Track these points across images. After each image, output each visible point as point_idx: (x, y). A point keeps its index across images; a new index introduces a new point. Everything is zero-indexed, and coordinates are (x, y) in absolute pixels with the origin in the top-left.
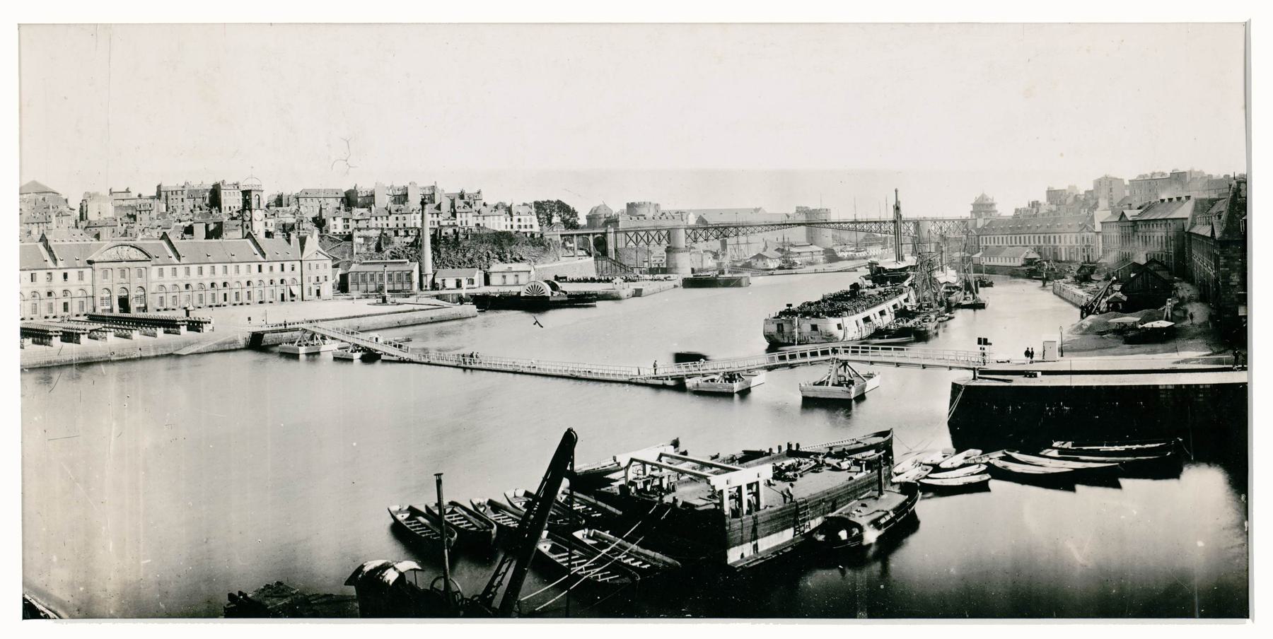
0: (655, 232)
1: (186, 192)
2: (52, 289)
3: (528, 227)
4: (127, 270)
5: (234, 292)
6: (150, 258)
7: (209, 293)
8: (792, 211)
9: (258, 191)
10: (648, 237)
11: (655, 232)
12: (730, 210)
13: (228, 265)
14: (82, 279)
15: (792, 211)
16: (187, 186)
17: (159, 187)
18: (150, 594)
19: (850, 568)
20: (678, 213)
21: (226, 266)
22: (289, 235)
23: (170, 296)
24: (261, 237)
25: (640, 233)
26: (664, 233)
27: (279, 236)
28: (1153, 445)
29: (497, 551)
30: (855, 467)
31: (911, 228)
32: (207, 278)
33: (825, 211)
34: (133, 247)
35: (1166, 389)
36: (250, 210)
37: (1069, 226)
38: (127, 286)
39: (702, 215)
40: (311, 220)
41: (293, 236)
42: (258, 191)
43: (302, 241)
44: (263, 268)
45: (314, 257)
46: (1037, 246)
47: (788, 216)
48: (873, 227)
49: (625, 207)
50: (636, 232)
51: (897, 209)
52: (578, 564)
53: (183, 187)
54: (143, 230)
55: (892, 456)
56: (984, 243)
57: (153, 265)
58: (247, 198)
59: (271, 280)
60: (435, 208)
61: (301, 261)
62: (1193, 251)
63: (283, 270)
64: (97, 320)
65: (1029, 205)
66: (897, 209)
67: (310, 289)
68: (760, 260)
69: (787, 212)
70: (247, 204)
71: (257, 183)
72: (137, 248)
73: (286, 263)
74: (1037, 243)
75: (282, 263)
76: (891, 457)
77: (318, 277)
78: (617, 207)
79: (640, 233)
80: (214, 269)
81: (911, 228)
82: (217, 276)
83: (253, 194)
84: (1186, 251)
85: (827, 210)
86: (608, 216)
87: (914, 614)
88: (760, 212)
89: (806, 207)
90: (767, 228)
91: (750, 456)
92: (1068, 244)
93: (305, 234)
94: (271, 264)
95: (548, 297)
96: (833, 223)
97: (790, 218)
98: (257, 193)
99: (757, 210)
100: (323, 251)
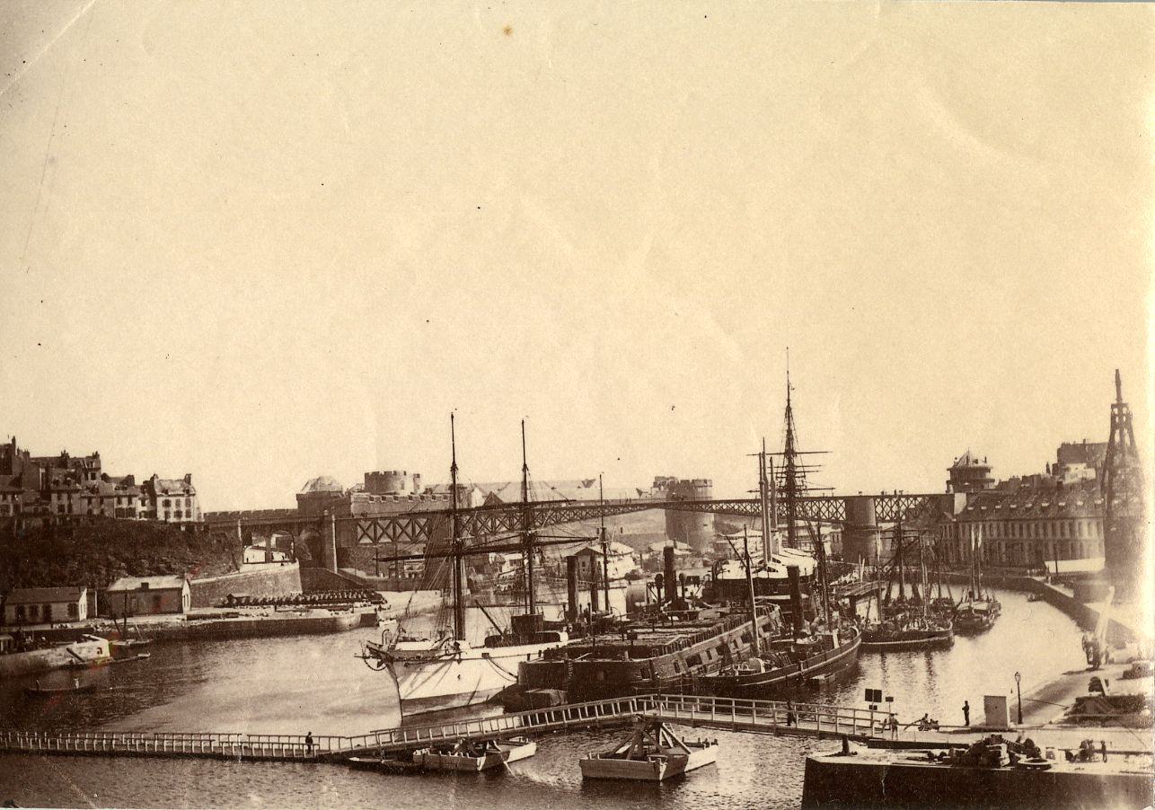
0: (388, 522)
3: (184, 514)
8: (647, 485)
10: (394, 529)
15: (647, 485)
18: (136, 773)
25: (401, 521)
31: (841, 510)
47: (640, 492)
48: (824, 509)
49: (362, 480)
50: (394, 521)
51: (454, 468)
52: (406, 768)
60: (10, 484)
64: (908, 650)
65: (1048, 470)
66: (454, 468)
74: (1059, 536)
79: (401, 521)
81: (841, 510)
84: (271, 522)
85: (705, 481)
91: (944, 732)
97: (643, 496)
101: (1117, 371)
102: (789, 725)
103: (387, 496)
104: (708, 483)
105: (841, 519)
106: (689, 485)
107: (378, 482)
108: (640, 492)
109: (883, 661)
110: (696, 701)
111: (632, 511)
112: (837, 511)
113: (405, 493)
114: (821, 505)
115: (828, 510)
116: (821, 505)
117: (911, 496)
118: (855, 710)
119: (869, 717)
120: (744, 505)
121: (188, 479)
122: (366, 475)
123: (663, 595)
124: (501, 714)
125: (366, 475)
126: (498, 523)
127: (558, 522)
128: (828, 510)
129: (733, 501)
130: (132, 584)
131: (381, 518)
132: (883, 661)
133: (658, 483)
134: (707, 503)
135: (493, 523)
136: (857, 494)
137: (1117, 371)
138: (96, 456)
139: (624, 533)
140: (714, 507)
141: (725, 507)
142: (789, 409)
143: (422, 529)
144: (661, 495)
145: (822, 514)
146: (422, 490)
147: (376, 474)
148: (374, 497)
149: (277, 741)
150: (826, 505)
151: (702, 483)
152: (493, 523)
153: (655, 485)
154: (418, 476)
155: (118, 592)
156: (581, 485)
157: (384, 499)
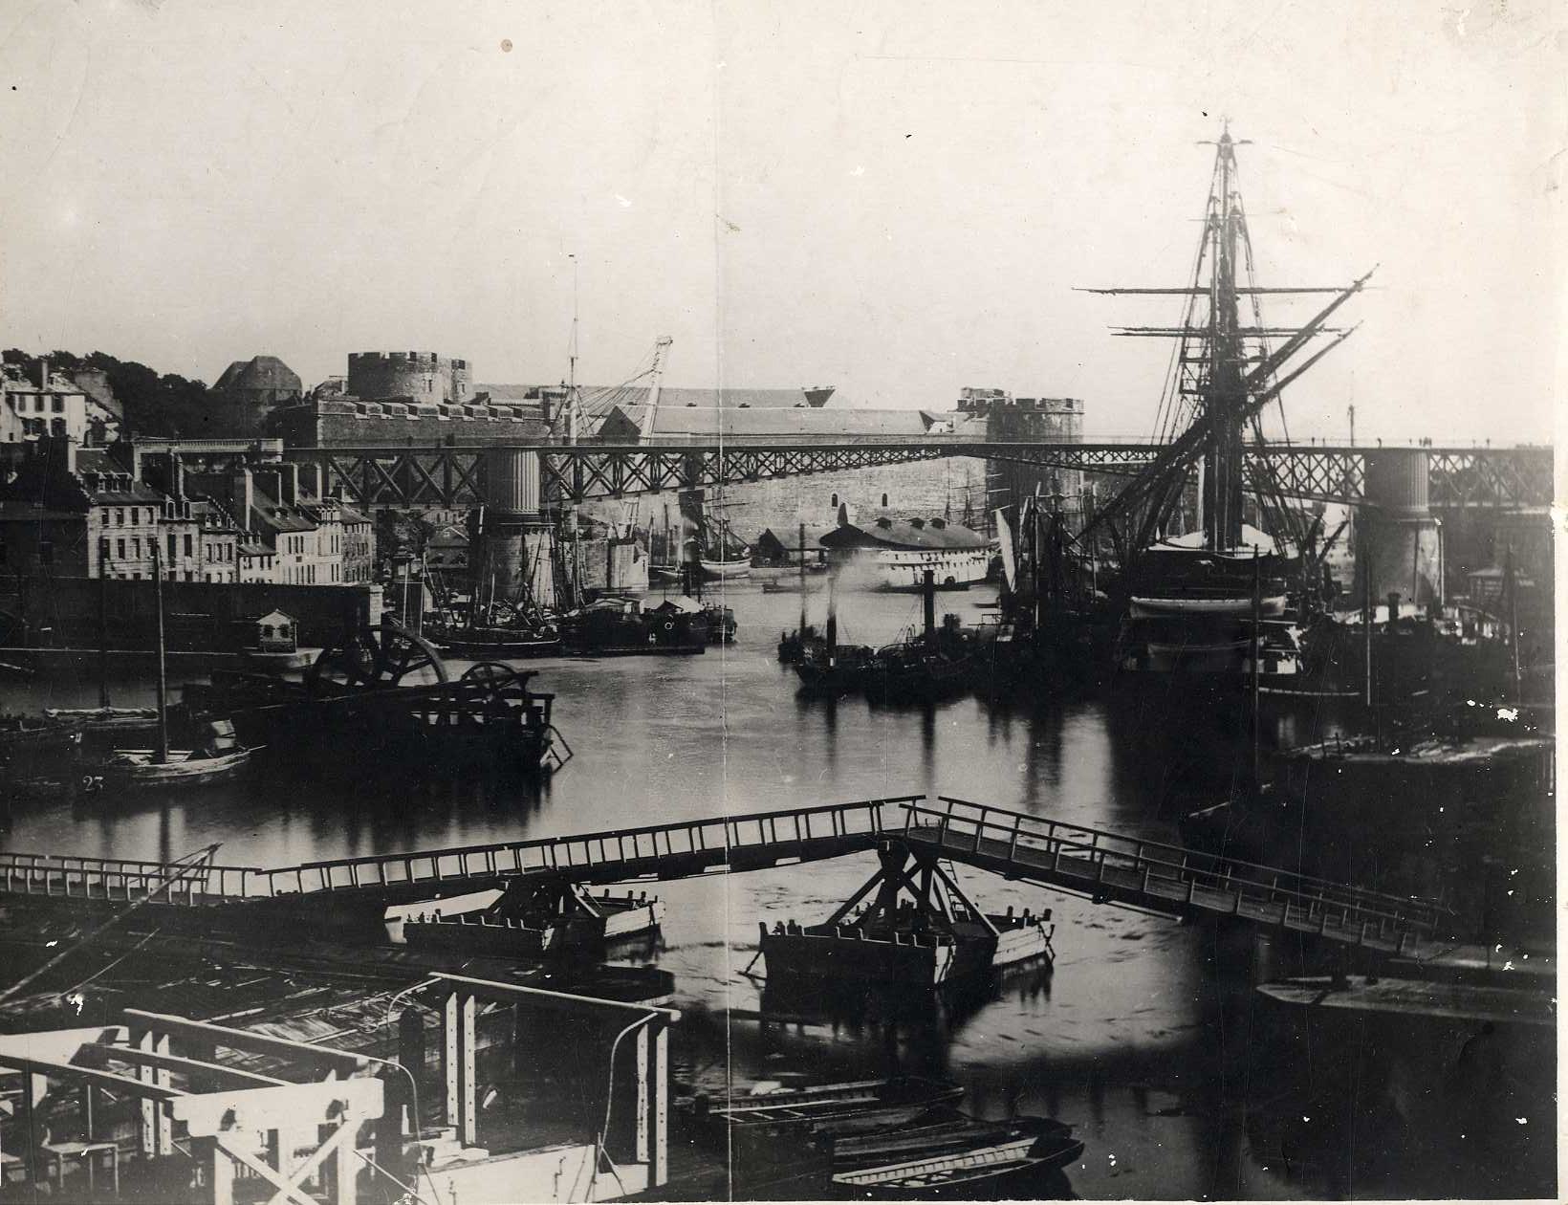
0: (432, 460)
11: (565, 458)
19: (845, 1027)
25: (420, 460)
29: (1015, 988)
30: (1006, 934)
39: (622, 406)
47: (928, 421)
48: (1318, 474)
49: (342, 371)
55: (440, 899)
62: (18, 519)
69: (924, 409)
76: (438, 896)
85: (1069, 403)
86: (283, 396)
87: (62, 1021)
89: (999, 393)
90: (780, 463)
96: (1094, 448)
97: (935, 429)
99: (818, 398)
103: (394, 405)
104: (1076, 407)
105: (1317, 490)
106: (1031, 411)
110: (1341, 914)
111: (909, 459)
112: (1310, 476)
114: (1314, 463)
115: (1327, 473)
116: (1314, 463)
117: (1436, 451)
118: (1053, 824)
119: (1013, 826)
120: (1100, 454)
125: (352, 357)
128: (1310, 472)
130: (1460, 598)
133: (971, 406)
134: (1071, 449)
135: (578, 473)
136: (1376, 445)
139: (890, 506)
140: (1085, 457)
141: (1108, 460)
142: (1091, 291)
143: (465, 478)
144: (974, 429)
145: (1313, 484)
146: (466, 397)
148: (368, 405)
149: (137, 872)
150: (1324, 464)
151: (1062, 407)
152: (578, 473)
153: (962, 406)
154: (462, 364)
155: (317, 647)
156: (804, 401)
157: (387, 410)
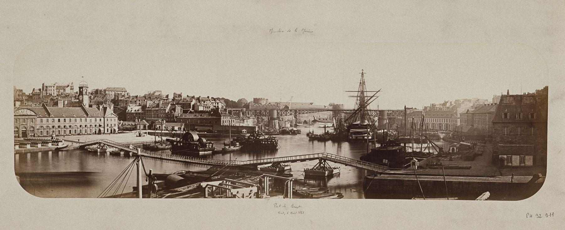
1: (55, 87)
2: (82, 125)
4: (26, 119)
5: (74, 130)
6: (36, 114)
7: (63, 130)
8: (327, 105)
9: (86, 87)
12: (300, 103)
13: (72, 118)
14: (96, 121)
16: (56, 84)
17: (43, 84)
20: (276, 103)
21: (86, 119)
22: (99, 106)
23: (45, 131)
24: (87, 107)
26: (268, 111)
27: (95, 107)
28: (231, 180)
32: (62, 124)
33: (342, 105)
34: (29, 110)
35: (456, 183)
36: (82, 95)
37: (433, 115)
38: (26, 126)
40: (111, 100)
41: (101, 107)
42: (86, 87)
43: (105, 109)
44: (108, 120)
45: (110, 116)
46: (446, 124)
48: (373, 113)
53: (54, 84)
54: (338, 76)
56: (432, 122)
57: (38, 118)
58: (81, 90)
59: (115, 124)
61: (104, 118)
63: (65, 121)
67: (108, 129)
68: (226, 125)
70: (81, 93)
71: (86, 84)
72: (31, 110)
73: (61, 119)
74: (446, 122)
75: (59, 118)
77: (115, 124)
78: (250, 100)
80: (48, 120)
82: (43, 123)
83: (84, 88)
85: (342, 105)
88: (313, 105)
90: (307, 112)
92: (426, 122)
93: (106, 106)
94: (91, 118)
95: (415, 143)
96: (345, 110)
97: (326, 108)
98: (85, 88)
99: (311, 104)
100: (114, 114)
101: (508, 90)
102: (226, 183)
107: (256, 100)
108: (325, 107)
109: (162, 163)
113: (264, 104)
121: (187, 95)
122: (254, 98)
123: (246, 138)
124: (334, 170)
126: (287, 113)
127: (303, 113)
129: (346, 110)
131: (252, 110)
132: (162, 163)
134: (343, 110)
137: (508, 90)
138: (546, 89)
144: (331, 108)
147: (256, 98)
151: (342, 105)
153: (329, 105)
154: (267, 99)
